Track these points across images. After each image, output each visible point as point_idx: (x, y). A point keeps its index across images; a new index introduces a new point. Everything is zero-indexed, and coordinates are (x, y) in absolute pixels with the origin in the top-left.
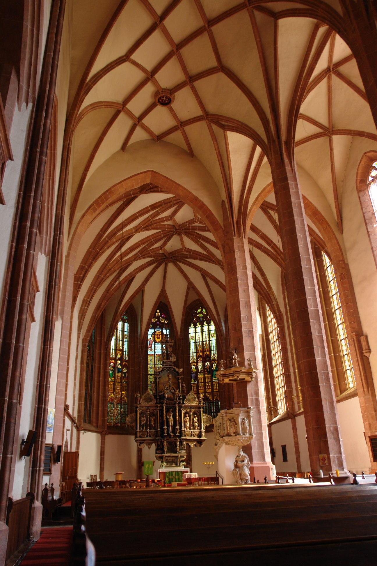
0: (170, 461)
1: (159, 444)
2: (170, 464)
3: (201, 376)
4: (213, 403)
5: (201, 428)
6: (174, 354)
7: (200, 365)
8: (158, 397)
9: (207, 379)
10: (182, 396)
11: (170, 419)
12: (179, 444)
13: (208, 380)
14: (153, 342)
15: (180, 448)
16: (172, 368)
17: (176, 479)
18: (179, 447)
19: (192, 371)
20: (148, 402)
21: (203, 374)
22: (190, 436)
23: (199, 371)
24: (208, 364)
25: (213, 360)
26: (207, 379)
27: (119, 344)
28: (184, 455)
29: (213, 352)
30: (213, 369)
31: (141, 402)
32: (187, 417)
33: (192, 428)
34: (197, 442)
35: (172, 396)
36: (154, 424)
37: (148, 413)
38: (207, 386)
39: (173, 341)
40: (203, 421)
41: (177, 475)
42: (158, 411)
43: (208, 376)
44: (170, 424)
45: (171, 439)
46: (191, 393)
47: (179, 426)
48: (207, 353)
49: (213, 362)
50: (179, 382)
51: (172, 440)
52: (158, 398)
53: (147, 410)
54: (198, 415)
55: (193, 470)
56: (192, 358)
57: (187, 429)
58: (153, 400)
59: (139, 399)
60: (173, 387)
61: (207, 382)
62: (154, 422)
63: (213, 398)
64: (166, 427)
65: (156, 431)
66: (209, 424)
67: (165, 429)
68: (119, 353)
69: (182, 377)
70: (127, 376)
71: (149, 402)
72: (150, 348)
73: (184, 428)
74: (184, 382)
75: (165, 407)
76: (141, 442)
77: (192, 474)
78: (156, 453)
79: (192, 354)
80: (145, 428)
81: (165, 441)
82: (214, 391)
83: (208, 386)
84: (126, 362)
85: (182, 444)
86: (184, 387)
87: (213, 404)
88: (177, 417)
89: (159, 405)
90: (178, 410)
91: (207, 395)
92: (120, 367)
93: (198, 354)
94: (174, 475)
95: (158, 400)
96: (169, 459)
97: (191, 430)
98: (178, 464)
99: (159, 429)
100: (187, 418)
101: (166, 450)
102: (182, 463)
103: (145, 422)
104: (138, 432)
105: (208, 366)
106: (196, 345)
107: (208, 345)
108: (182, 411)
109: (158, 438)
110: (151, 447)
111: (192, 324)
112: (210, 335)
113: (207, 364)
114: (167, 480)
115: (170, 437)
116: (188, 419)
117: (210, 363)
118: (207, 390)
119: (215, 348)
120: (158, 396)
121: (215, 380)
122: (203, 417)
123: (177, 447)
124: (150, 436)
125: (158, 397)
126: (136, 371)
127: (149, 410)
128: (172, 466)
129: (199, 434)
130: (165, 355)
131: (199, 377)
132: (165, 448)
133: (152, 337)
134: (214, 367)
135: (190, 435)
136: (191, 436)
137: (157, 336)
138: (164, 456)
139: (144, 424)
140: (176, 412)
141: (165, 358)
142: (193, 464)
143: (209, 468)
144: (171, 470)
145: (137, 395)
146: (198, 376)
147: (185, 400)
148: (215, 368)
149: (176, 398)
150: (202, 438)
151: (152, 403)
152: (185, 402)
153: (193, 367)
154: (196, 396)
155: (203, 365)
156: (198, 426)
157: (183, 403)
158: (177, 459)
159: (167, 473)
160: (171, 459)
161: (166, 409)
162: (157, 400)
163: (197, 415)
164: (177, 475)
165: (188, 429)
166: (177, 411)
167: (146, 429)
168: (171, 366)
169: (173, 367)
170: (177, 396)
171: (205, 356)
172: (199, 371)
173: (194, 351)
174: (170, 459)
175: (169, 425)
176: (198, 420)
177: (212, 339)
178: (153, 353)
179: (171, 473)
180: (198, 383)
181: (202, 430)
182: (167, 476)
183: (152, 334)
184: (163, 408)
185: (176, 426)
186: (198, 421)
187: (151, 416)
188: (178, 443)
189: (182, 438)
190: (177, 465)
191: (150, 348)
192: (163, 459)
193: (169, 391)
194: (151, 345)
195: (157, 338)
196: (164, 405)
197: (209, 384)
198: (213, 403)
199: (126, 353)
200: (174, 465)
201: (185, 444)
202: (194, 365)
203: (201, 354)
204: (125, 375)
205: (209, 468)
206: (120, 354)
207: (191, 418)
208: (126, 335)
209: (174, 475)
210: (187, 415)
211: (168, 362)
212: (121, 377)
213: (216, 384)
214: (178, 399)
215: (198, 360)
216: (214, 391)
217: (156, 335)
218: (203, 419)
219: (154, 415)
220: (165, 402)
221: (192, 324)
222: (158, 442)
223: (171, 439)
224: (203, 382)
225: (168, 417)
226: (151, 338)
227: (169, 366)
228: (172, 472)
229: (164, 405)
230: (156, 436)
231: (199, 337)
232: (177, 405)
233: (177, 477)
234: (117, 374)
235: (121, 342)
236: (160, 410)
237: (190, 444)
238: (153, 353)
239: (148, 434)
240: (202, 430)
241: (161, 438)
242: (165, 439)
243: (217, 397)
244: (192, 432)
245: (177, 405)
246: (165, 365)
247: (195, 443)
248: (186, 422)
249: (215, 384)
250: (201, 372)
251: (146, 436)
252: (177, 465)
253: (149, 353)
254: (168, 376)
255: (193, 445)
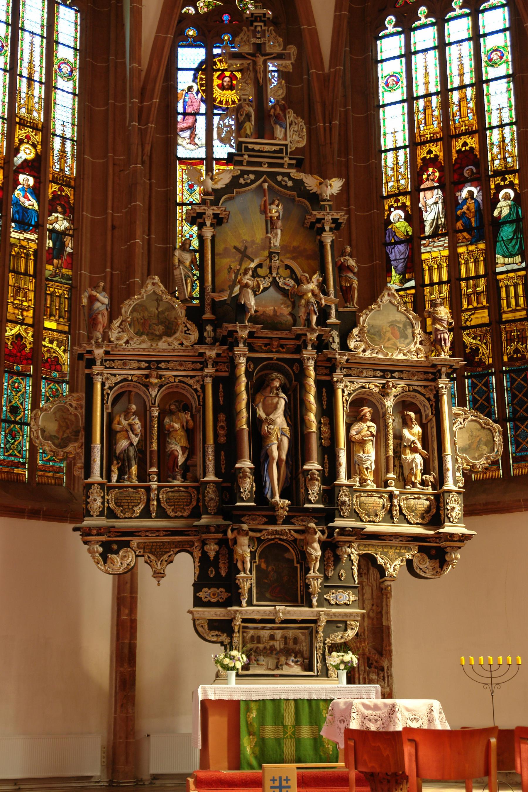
0: (272, 649)
1: (212, 554)
2: (272, 662)
3: (434, 255)
4: (499, 374)
5: (441, 480)
6: (298, 113)
7: (430, 202)
8: (208, 316)
9: (467, 263)
10: (339, 315)
11: (273, 422)
12: (319, 553)
13: (472, 267)
14: (203, 108)
15: (326, 578)
16: (288, 175)
17: (298, 741)
18: (323, 569)
19: (394, 234)
20: (156, 338)
21: (445, 241)
22: (384, 521)
23: (428, 230)
24: (471, 193)
25: (497, 173)
26: (467, 263)
27: (29, 97)
28: (351, 614)
29: (494, 136)
30: (496, 213)
31: (113, 335)
32: (363, 419)
33: (391, 475)
34: (421, 550)
35: (285, 311)
36: (183, 449)
37: (154, 392)
38: (469, 296)
39: (293, 50)
40: (454, 444)
41: (269, 718)
42: (209, 381)
43: (470, 253)
44: (274, 448)
45: (278, 528)
46: (386, 298)
47: (322, 464)
48: (465, 144)
49: (498, 180)
50: (322, 245)
51: (281, 533)
52: (209, 322)
53: (147, 376)
54: (428, 412)
55: (396, 688)
56: (390, 173)
57: (363, 482)
58: (181, 328)
59: (103, 319)
60: (287, 267)
61: (468, 279)
62: (184, 442)
63: (497, 352)
64: (246, 464)
65: (197, 488)
66: (483, 461)
67: (245, 476)
68: (28, 137)
69: (341, 216)
70: (69, 250)
71: (160, 337)
72: (187, 134)
73: (349, 477)
74: (349, 249)
75: (243, 360)
76: (137, 556)
77: (401, 703)
78: (198, 602)
79: (390, 155)
80: (134, 469)
81: (244, 540)
82: (505, 317)
83: (474, 299)
84: (68, 186)
85: (337, 559)
86: (349, 269)
87: (499, 382)
88: (312, 417)
89: (211, 353)
90: (317, 382)
91: (467, 340)
92: (31, 203)
93: (422, 153)
94: (289, 720)
95: (209, 328)
96: (265, 634)
97: (386, 485)
98: (317, 665)
99: (211, 477)
100: (364, 426)
101: (247, 587)
102: (334, 658)
103: (135, 440)
104: (96, 489)
105: (471, 204)
106: (411, 113)
107: (472, 105)
108: (340, 386)
109: (204, 520)
110: (169, 569)
111: (390, 20)
112: (484, 58)
113: (464, 193)
114: (248, 750)
115: (273, 520)
116: (374, 430)
117: (485, 190)
118: (465, 316)
119: (508, 116)
120: (208, 309)
121: (510, 267)
122: (452, 425)
123: (312, 574)
124: (162, 514)
125: (208, 316)
126: (113, 227)
127: (160, 377)
128: (286, 671)
129: (429, 508)
130: (248, 116)
131: (424, 257)
132: (242, 575)
133: (194, 81)
134: (501, 204)
135: (382, 513)
136: (390, 516)
137: (220, 77)
138: (239, 617)
139: (132, 453)
140: (303, 389)
141: (249, 127)
142: (395, 671)
143: (492, 687)
144: (295, 691)
145: (92, 299)
146: (420, 253)
147: (355, 331)
148: (506, 211)
149: (302, 313)
150: (448, 529)
151: (176, 344)
152: (352, 344)
153: (397, 215)
154: (412, 315)
155: (444, 203)
156: (426, 471)
157: (344, 346)
158: (312, 634)
159: (248, 710)
160: (279, 634)
161: (248, 374)
162: (201, 331)
163: (418, 412)
164: (269, 718)
165: (371, 485)
166: (311, 382)
167: (143, 476)
168: (281, 166)
169: (293, 172)
170: (308, 302)
171: (455, 156)
172: (428, 230)
173: (403, 139)
174: (272, 637)
175: (268, 456)
176: (424, 439)
177: (489, 73)
178: (201, 153)
179: (270, 707)
180: (420, 286)
181: (449, 485)
182: (249, 725)
183: (197, 70)
184: (233, 366)
185: (306, 459)
186: (425, 446)
187: (171, 413)
188: (316, 551)
189: (338, 523)
190: (309, 667)
191: (187, 134)
192: (230, 632)
193: (264, 284)
194: (190, 120)
195: (222, 87)
196: (241, 349)
197: (475, 286)
198: (499, 374)
199: (63, 145)
200: (297, 670)
201: (355, 558)
202: (403, 207)
203: (437, 149)
204: (59, 246)
205: (492, 687)
206: (34, 146)
207: (386, 426)
208: (65, 61)
209: (289, 720)
210: (367, 410)
211: (267, 148)
212: (36, 252)
213: (516, 286)
214: (314, 318)
215: (422, 182)
216: (505, 317)
217: (216, 74)
218: (453, 434)
219: (186, 407)
220: (244, 334)
221: (390, 20)
222: (204, 543)
223: (278, 528)
224: (445, 278)
225: (261, 413)
226: (190, 88)
227: (270, 165)
228: (276, 702)
229: (237, 351)
230: (196, 514)
231: (427, 74)
232: (309, 353)
233: (305, 732)
234: (14, 235)
235: (38, 90)
236: (216, 381)
237: (380, 561)
238: (201, 153)
239: (149, 500)
240: (445, 487)
241: (220, 521)
242: (245, 527)
243: (520, 346)
244: (391, 496)
245: (309, 353)
246: (250, 164)
247: (409, 556)
248: (362, 443)
249: (507, 287)
250: (435, 235)
251: (138, 510)
252: (309, 667)
253: (181, 153)
254: (264, 211)
255: (398, 562)
